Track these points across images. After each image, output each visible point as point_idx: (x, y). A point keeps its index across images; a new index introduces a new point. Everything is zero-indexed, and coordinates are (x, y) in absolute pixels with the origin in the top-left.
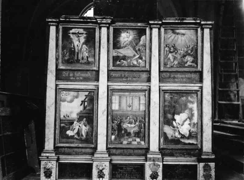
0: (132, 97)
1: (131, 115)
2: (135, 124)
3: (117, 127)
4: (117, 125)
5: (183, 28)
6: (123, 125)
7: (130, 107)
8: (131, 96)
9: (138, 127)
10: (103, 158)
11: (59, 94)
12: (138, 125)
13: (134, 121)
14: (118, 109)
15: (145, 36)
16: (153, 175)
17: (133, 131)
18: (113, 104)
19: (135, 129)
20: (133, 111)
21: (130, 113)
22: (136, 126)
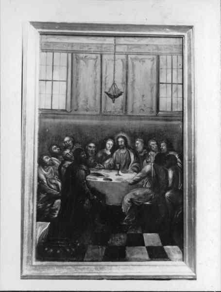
0: (124, 57)
1: (123, 131)
2: (137, 172)
3: (60, 184)
4: (60, 178)
5: (180, 277)
6: (88, 173)
7: (114, 97)
8: (121, 53)
9: (150, 180)
10: (139, 265)
11: (31, 173)
12: (149, 173)
13: (132, 157)
14: (62, 107)
15: (191, 29)
16: (163, 135)
17: (131, 201)
18: (53, 108)
19: (138, 192)
20: (129, 113)
21: (116, 123)
22: (142, 178)
